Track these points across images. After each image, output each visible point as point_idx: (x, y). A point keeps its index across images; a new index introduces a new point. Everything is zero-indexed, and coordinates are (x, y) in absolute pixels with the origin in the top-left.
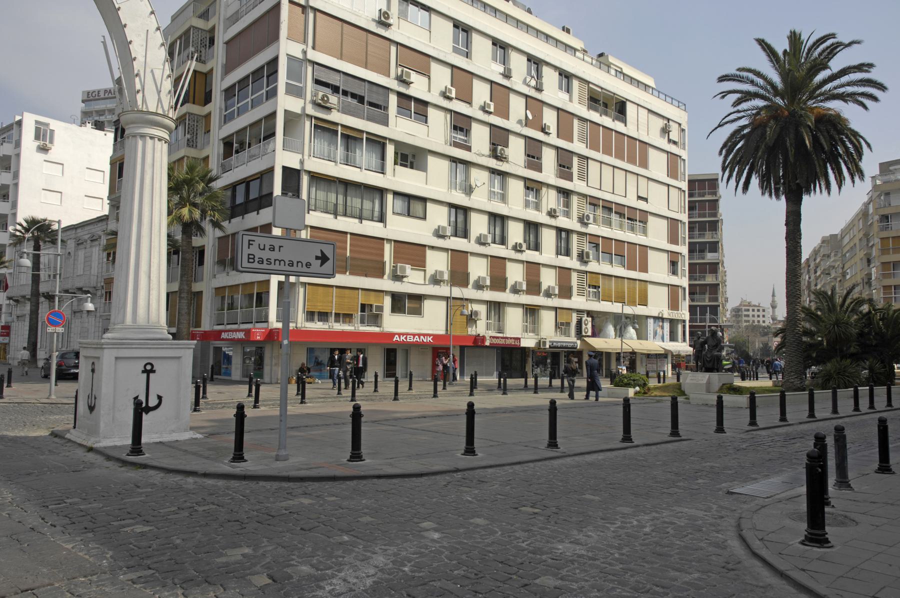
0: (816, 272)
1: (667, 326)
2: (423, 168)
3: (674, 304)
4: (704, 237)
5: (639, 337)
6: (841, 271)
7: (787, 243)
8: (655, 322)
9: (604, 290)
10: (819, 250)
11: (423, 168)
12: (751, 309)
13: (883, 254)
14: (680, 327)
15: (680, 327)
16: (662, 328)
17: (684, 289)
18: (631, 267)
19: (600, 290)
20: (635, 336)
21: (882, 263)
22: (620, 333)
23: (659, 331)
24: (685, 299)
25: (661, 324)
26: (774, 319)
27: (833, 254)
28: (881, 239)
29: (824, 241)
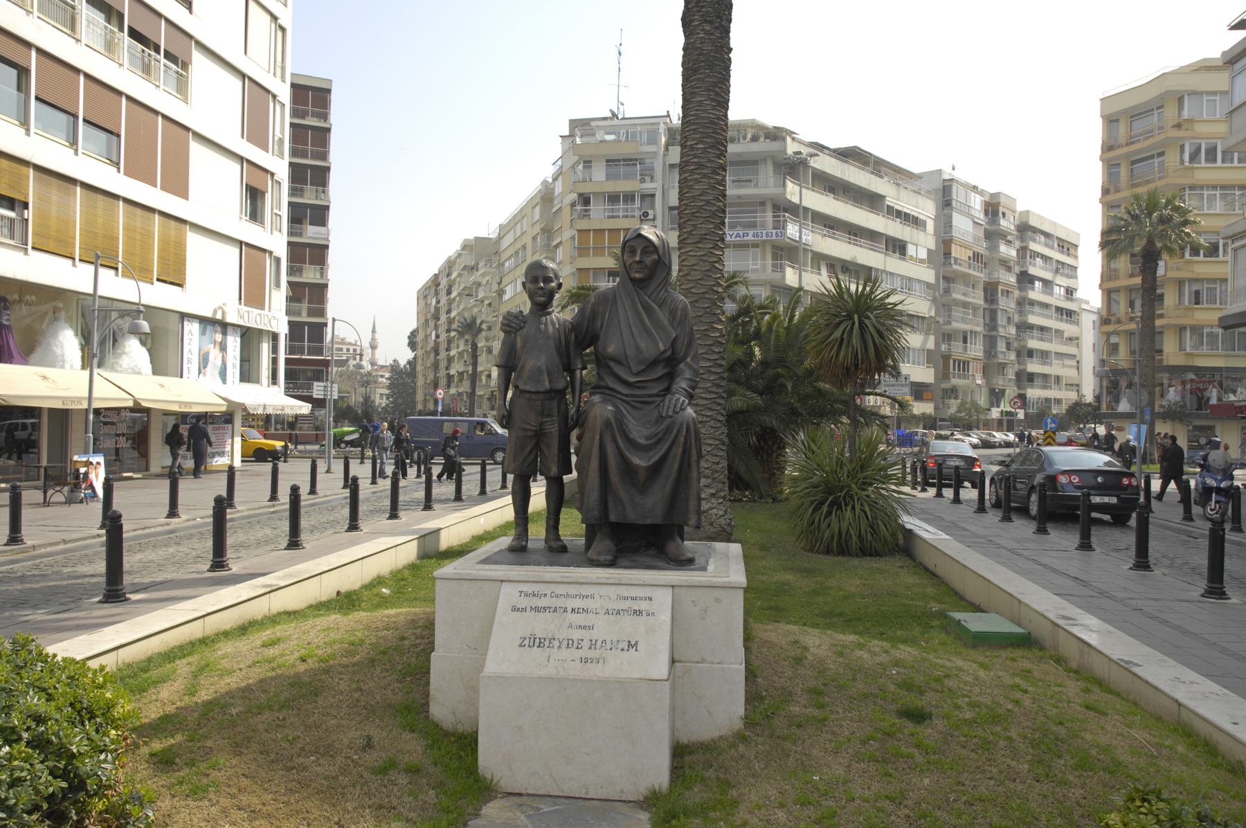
0: (449, 293)
1: (234, 343)
2: (83, 368)
3: (252, 294)
4: (302, 196)
5: (159, 368)
6: (495, 287)
7: (730, 14)
8: (203, 333)
9: (41, 215)
10: (454, 262)
11: (83, 368)
12: (345, 347)
13: (580, 256)
14: (265, 348)
15: (265, 348)
16: (223, 347)
17: (278, 261)
18: (140, 170)
19: (29, 214)
20: (147, 366)
21: (579, 269)
22: (96, 353)
23: (215, 356)
24: (278, 285)
25: (219, 337)
26: (373, 363)
27: (481, 264)
28: (579, 231)
29: (467, 246)
